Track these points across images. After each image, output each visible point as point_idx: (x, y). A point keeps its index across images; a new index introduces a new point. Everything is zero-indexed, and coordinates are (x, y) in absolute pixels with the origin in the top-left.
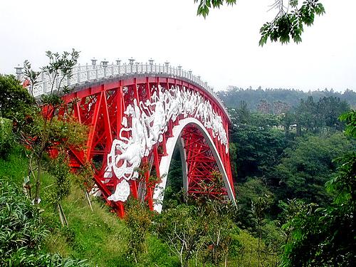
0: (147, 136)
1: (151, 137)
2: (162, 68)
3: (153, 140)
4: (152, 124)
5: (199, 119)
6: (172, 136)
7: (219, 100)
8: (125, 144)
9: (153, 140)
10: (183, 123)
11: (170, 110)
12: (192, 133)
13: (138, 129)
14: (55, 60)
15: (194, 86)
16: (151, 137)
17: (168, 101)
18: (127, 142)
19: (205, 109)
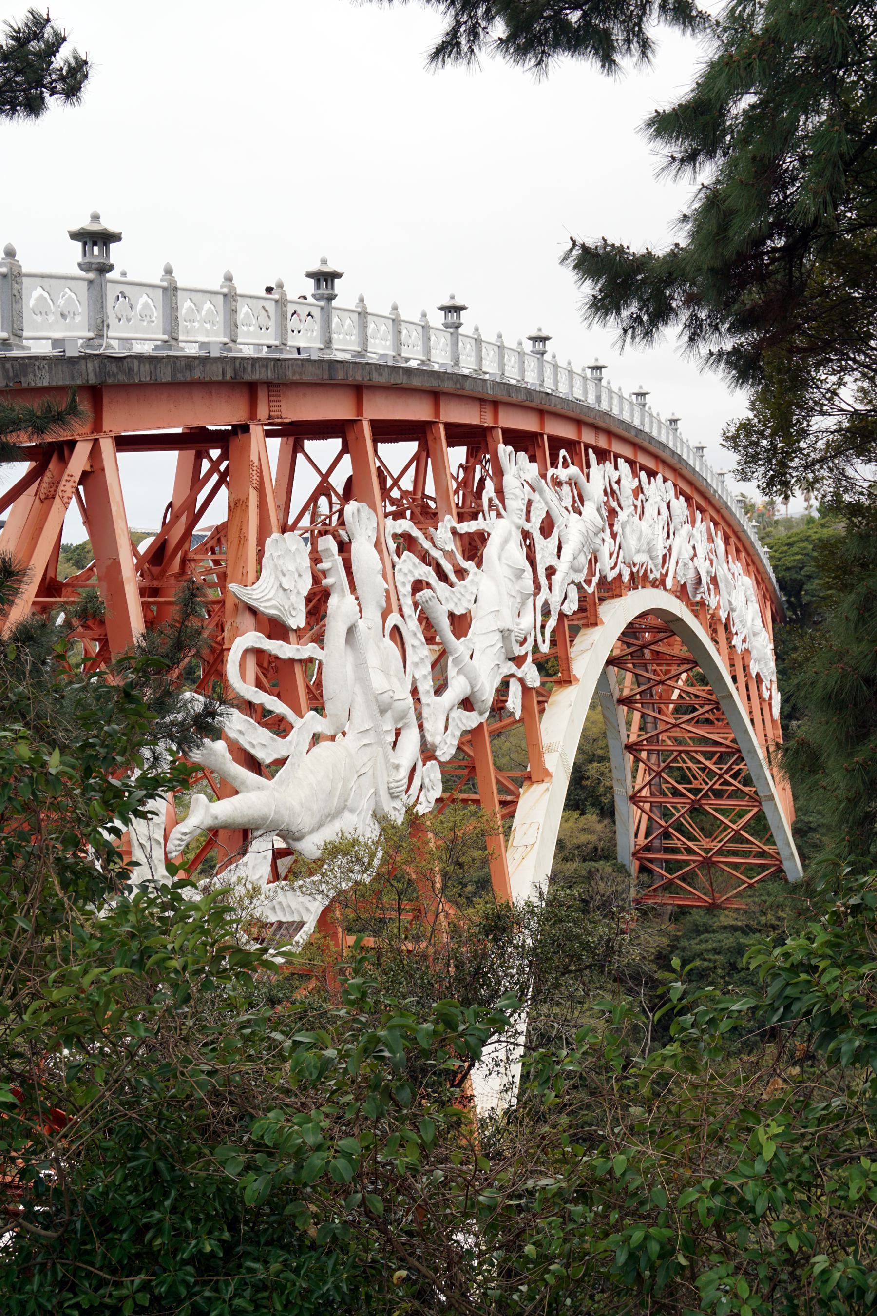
0: (426, 686)
1: (457, 688)
2: (511, 361)
3: (467, 704)
4: (460, 624)
5: (682, 592)
6: (567, 681)
7: (739, 513)
8: (264, 734)
9: (467, 704)
10: (617, 614)
11: (562, 567)
12: (651, 644)
13: (364, 664)
14: (95, 227)
15: (610, 434)
16: (457, 688)
17: (547, 528)
18: (280, 727)
19: (694, 547)
